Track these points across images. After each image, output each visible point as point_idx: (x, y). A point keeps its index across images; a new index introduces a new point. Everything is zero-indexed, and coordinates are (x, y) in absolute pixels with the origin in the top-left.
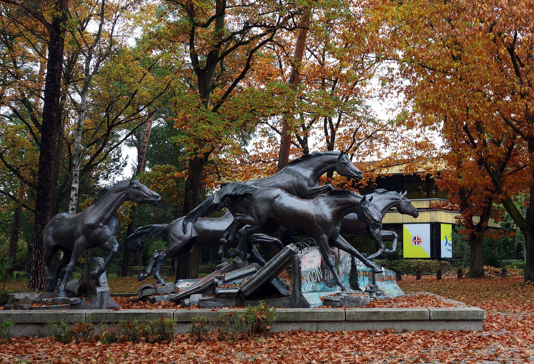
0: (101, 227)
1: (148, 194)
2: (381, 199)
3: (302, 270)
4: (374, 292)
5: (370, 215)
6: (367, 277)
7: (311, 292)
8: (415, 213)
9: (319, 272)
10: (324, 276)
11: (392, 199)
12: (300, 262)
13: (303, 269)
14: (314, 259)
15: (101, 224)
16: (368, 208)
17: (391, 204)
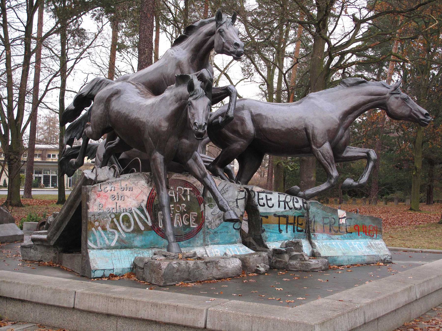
2: (347, 96)
4: (286, 252)
7: (115, 248)
8: (422, 117)
9: (142, 216)
11: (371, 94)
14: (127, 193)
16: (194, 102)
17: (364, 103)
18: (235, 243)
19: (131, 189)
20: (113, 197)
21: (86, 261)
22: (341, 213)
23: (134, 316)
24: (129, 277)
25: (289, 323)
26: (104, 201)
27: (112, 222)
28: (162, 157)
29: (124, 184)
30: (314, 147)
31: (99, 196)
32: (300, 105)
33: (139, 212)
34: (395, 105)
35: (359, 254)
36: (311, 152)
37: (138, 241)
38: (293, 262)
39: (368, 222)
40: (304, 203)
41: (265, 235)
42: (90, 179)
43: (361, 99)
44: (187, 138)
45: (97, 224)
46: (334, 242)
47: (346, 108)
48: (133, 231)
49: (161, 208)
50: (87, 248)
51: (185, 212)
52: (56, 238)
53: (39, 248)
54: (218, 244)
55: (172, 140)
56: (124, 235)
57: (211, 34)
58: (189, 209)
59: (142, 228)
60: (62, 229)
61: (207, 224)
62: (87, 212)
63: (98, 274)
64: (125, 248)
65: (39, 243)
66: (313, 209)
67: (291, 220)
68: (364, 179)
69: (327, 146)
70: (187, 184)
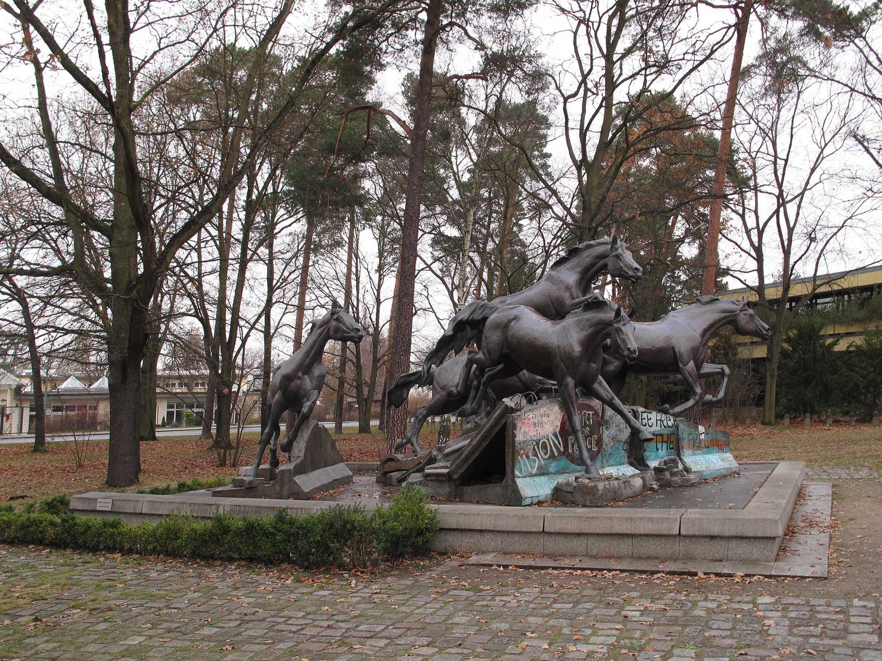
0: (299, 378)
1: (347, 328)
2: (704, 313)
3: (517, 439)
4: (667, 470)
5: (624, 341)
6: (665, 445)
7: (536, 475)
8: (765, 332)
9: (556, 442)
10: (566, 446)
11: (724, 311)
12: (514, 427)
13: (520, 437)
14: (545, 419)
15: (300, 374)
16: (623, 328)
17: (719, 320)
18: (622, 464)
19: (548, 416)
20: (535, 424)
21: (516, 491)
22: (701, 429)
23: (608, 532)
24: (552, 502)
25: (756, 520)
26: (527, 429)
27: (534, 449)
28: (573, 382)
29: (542, 410)
30: (681, 365)
31: (523, 424)
32: (665, 323)
33: (554, 438)
34: (744, 321)
35: (718, 467)
36: (678, 370)
37: (553, 467)
38: (675, 479)
39: (720, 437)
40: (675, 421)
41: (647, 454)
42: (511, 408)
43: (717, 316)
44: (594, 362)
45: (522, 452)
46: (697, 458)
47: (705, 326)
48: (549, 458)
49: (574, 432)
50: (513, 476)
51: (588, 436)
52: (461, 471)
53: (430, 484)
54: (612, 465)
55: (583, 365)
56: (543, 462)
57: (603, 256)
58: (591, 433)
59: (556, 454)
60: (471, 461)
61: (604, 446)
62: (514, 441)
63: (528, 501)
64: (543, 474)
65: (433, 478)
66: (681, 426)
67: (665, 439)
68: (721, 394)
69: (691, 364)
70: (590, 408)
